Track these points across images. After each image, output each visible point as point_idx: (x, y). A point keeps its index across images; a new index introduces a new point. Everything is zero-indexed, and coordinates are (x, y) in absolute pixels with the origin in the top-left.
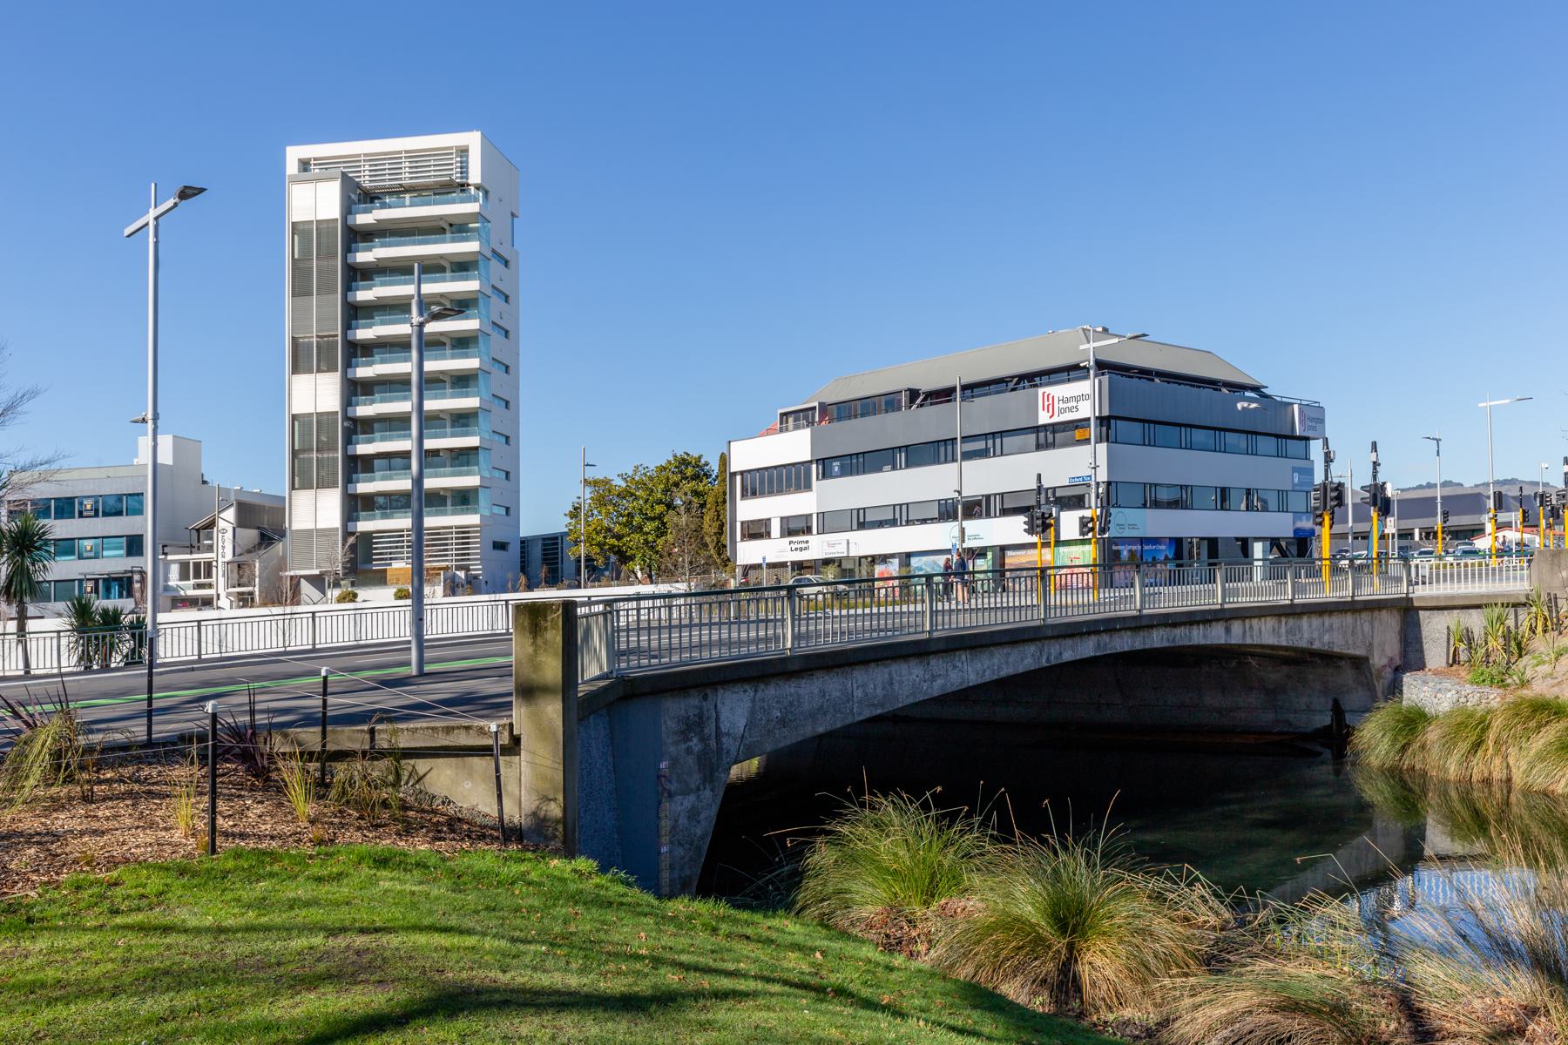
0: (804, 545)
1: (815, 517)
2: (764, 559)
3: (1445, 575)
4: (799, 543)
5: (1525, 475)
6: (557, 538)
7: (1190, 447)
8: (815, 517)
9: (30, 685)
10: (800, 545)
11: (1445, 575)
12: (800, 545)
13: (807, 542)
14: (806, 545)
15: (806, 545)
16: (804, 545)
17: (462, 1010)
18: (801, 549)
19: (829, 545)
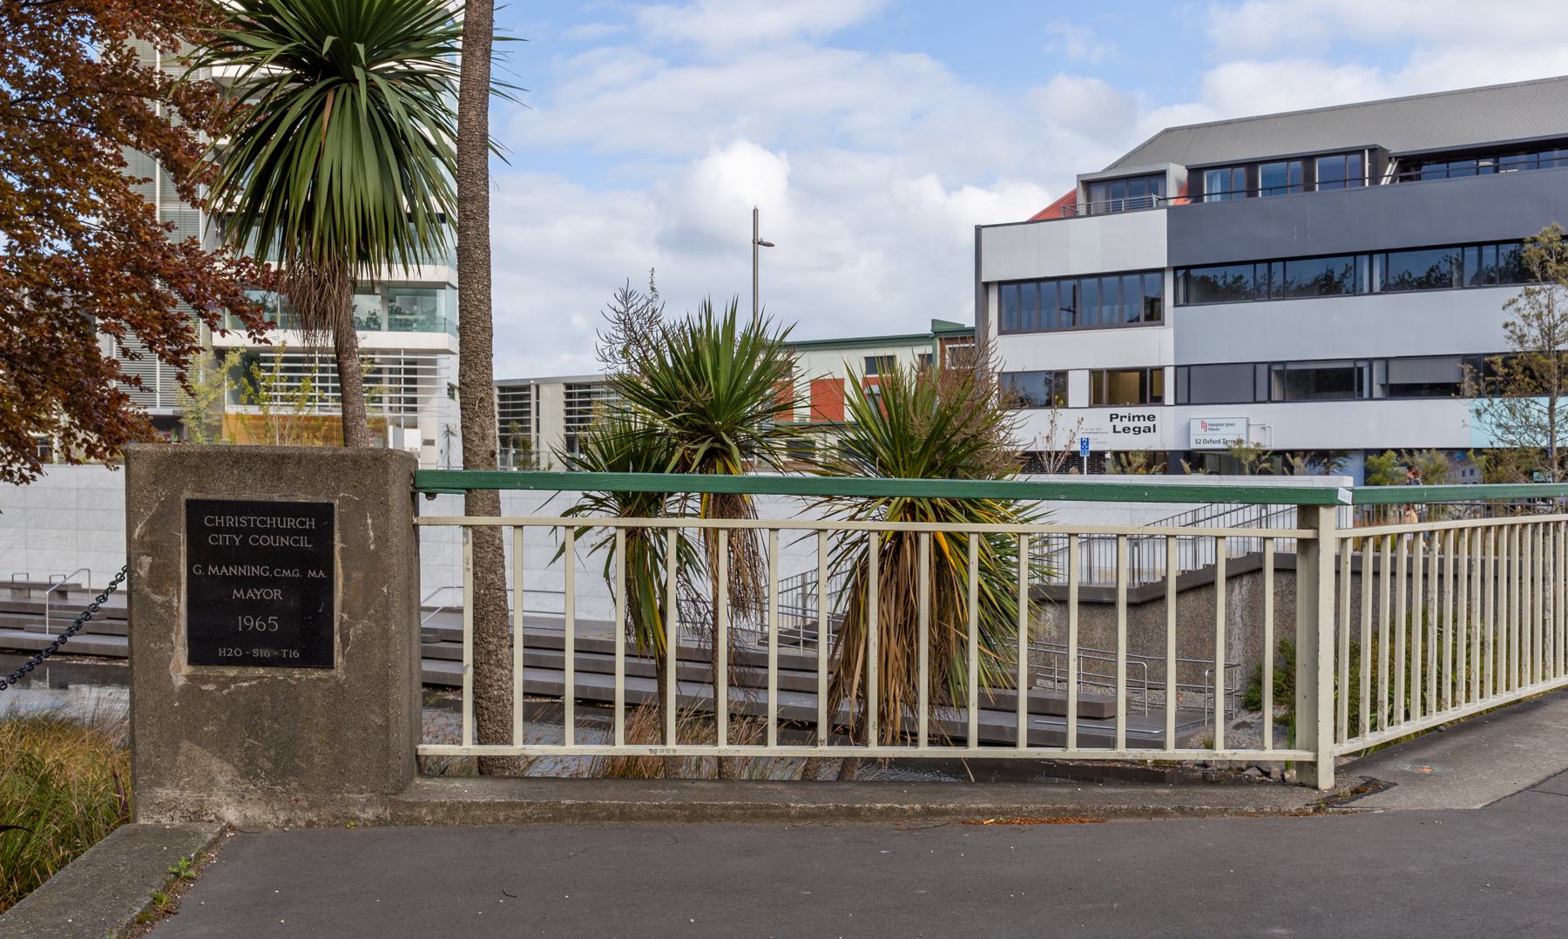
0: (1142, 424)
1: (1169, 376)
2: (1085, 443)
3: (581, 420)
4: (1131, 418)
5: (1379, 144)
6: (528, 388)
7: (1478, 171)
8: (1169, 376)
9: (1227, 657)
10: (1136, 423)
11: (581, 420)
12: (1136, 423)
13: (1151, 418)
14: (1150, 424)
15: (1150, 424)
16: (1142, 424)
17: (402, 457)
18: (1137, 431)
19: (1204, 426)
